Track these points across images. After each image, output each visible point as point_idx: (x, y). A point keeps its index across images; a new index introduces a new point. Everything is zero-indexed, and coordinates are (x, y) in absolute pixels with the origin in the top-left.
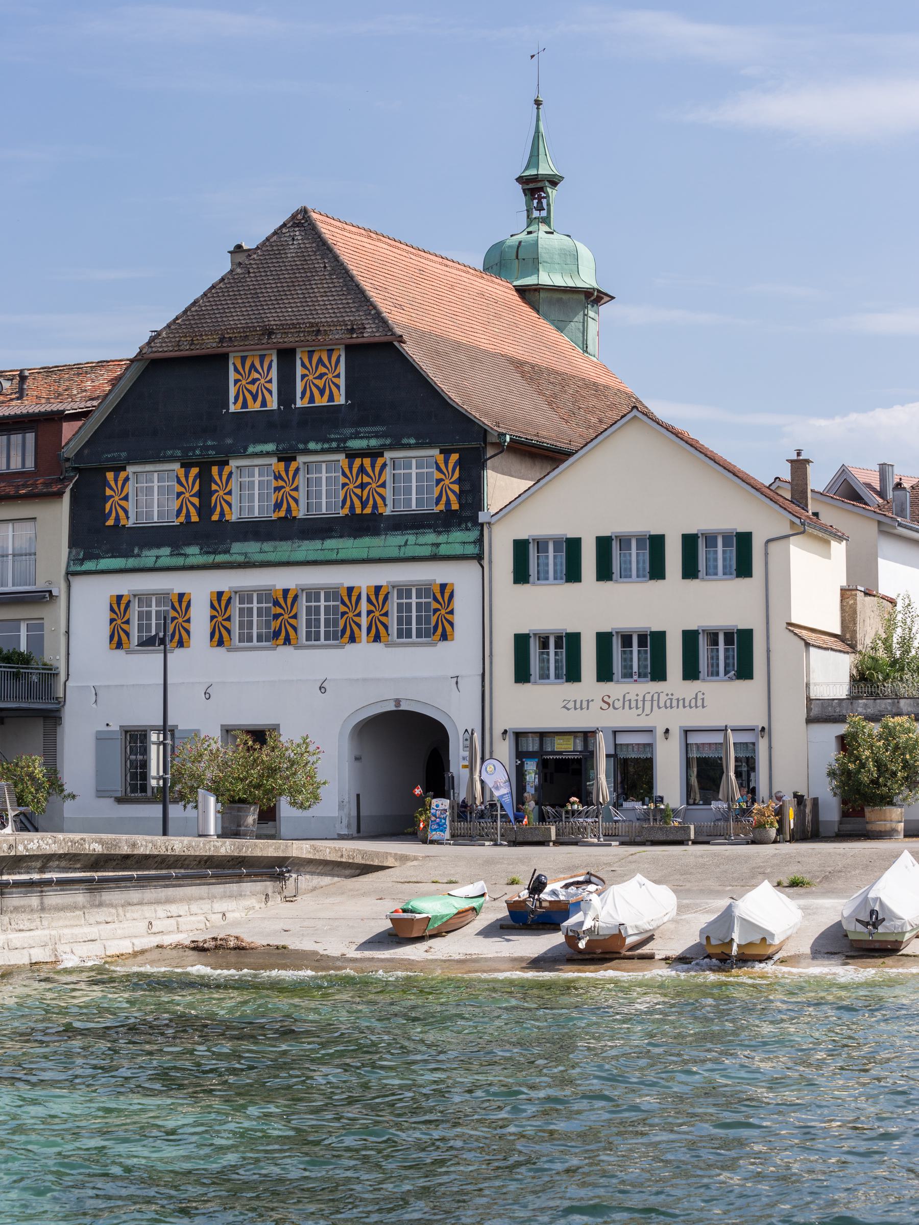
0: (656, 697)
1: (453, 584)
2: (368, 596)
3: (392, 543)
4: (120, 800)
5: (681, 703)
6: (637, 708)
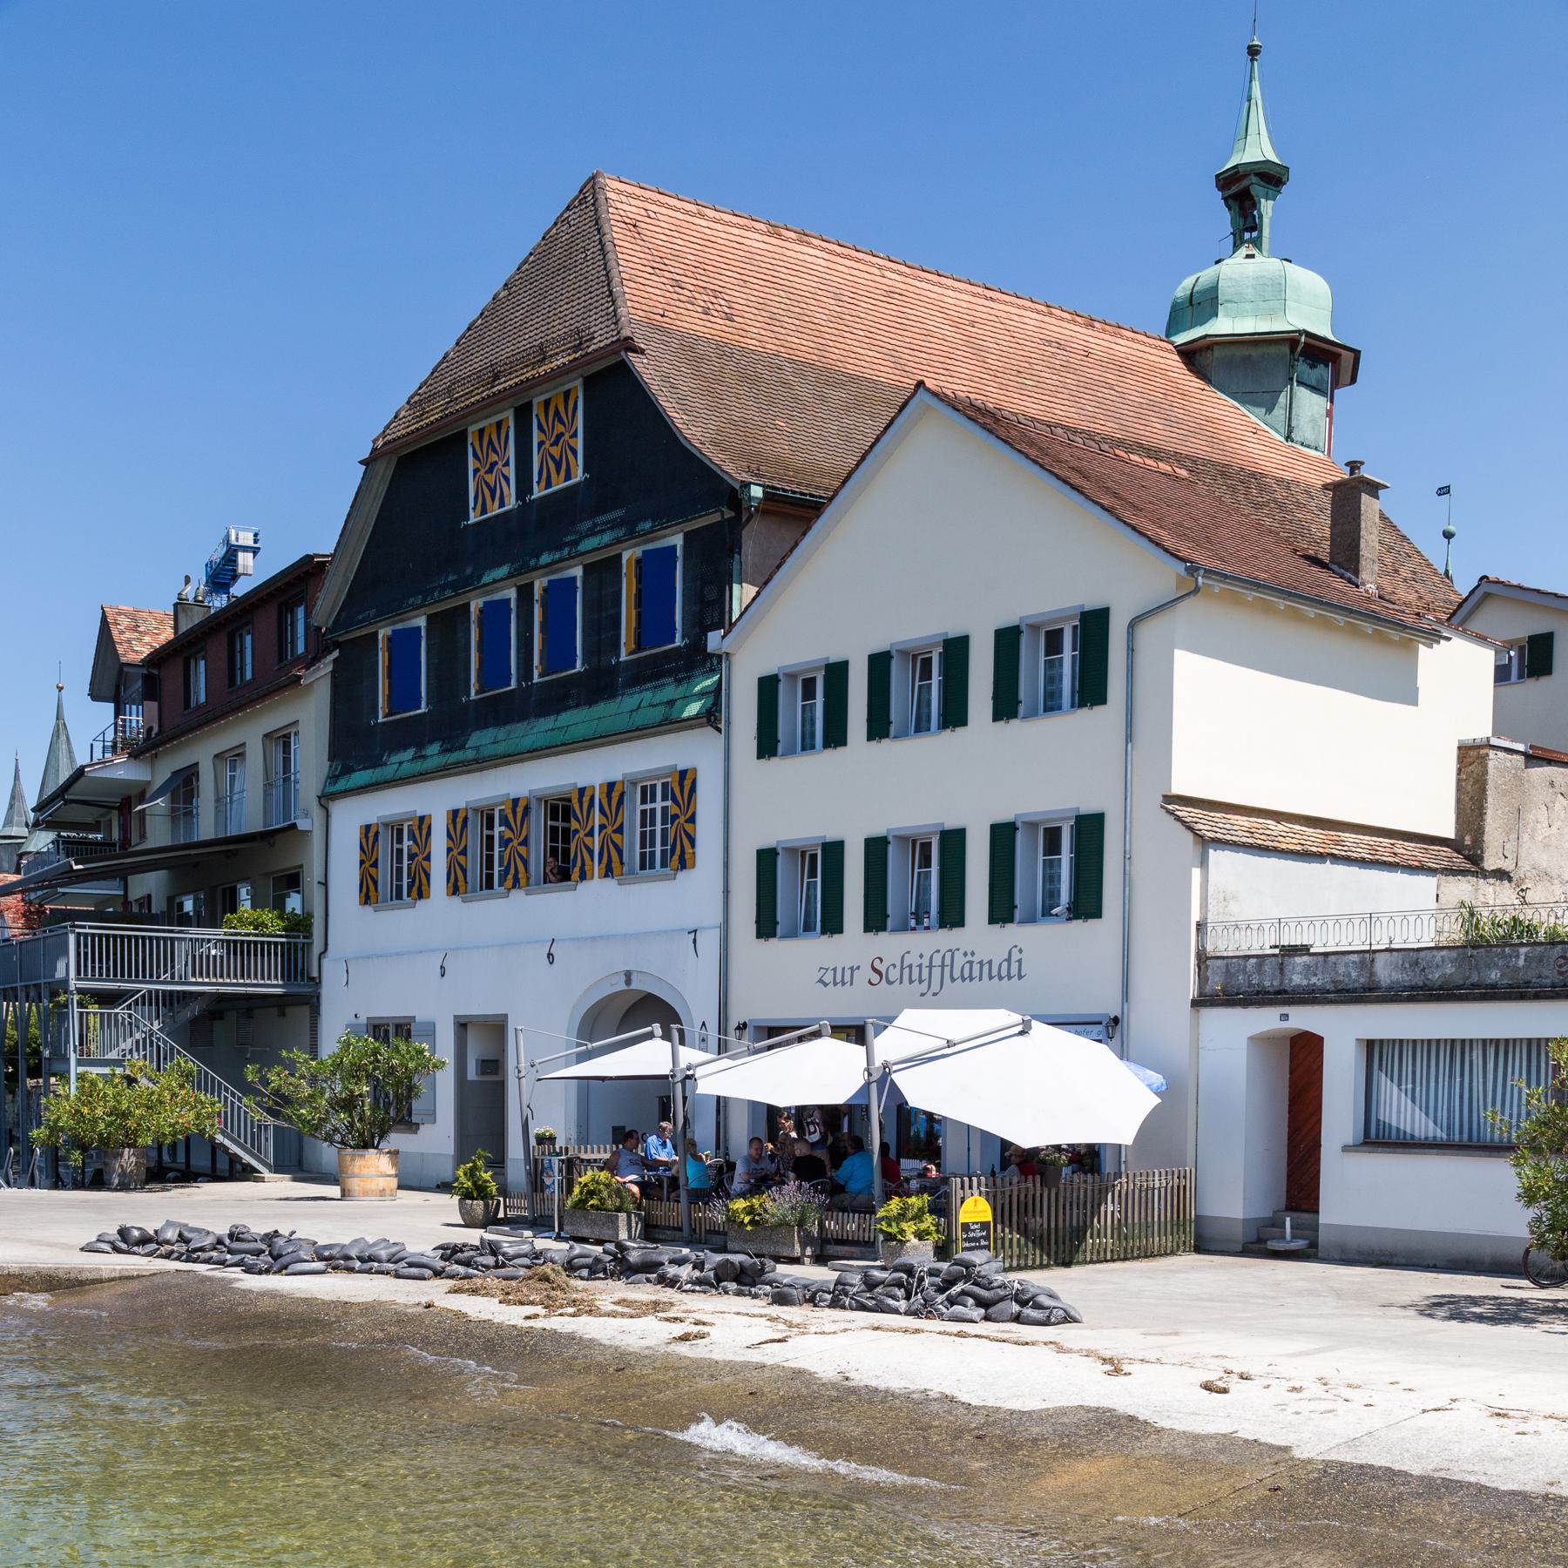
6: (921, 981)
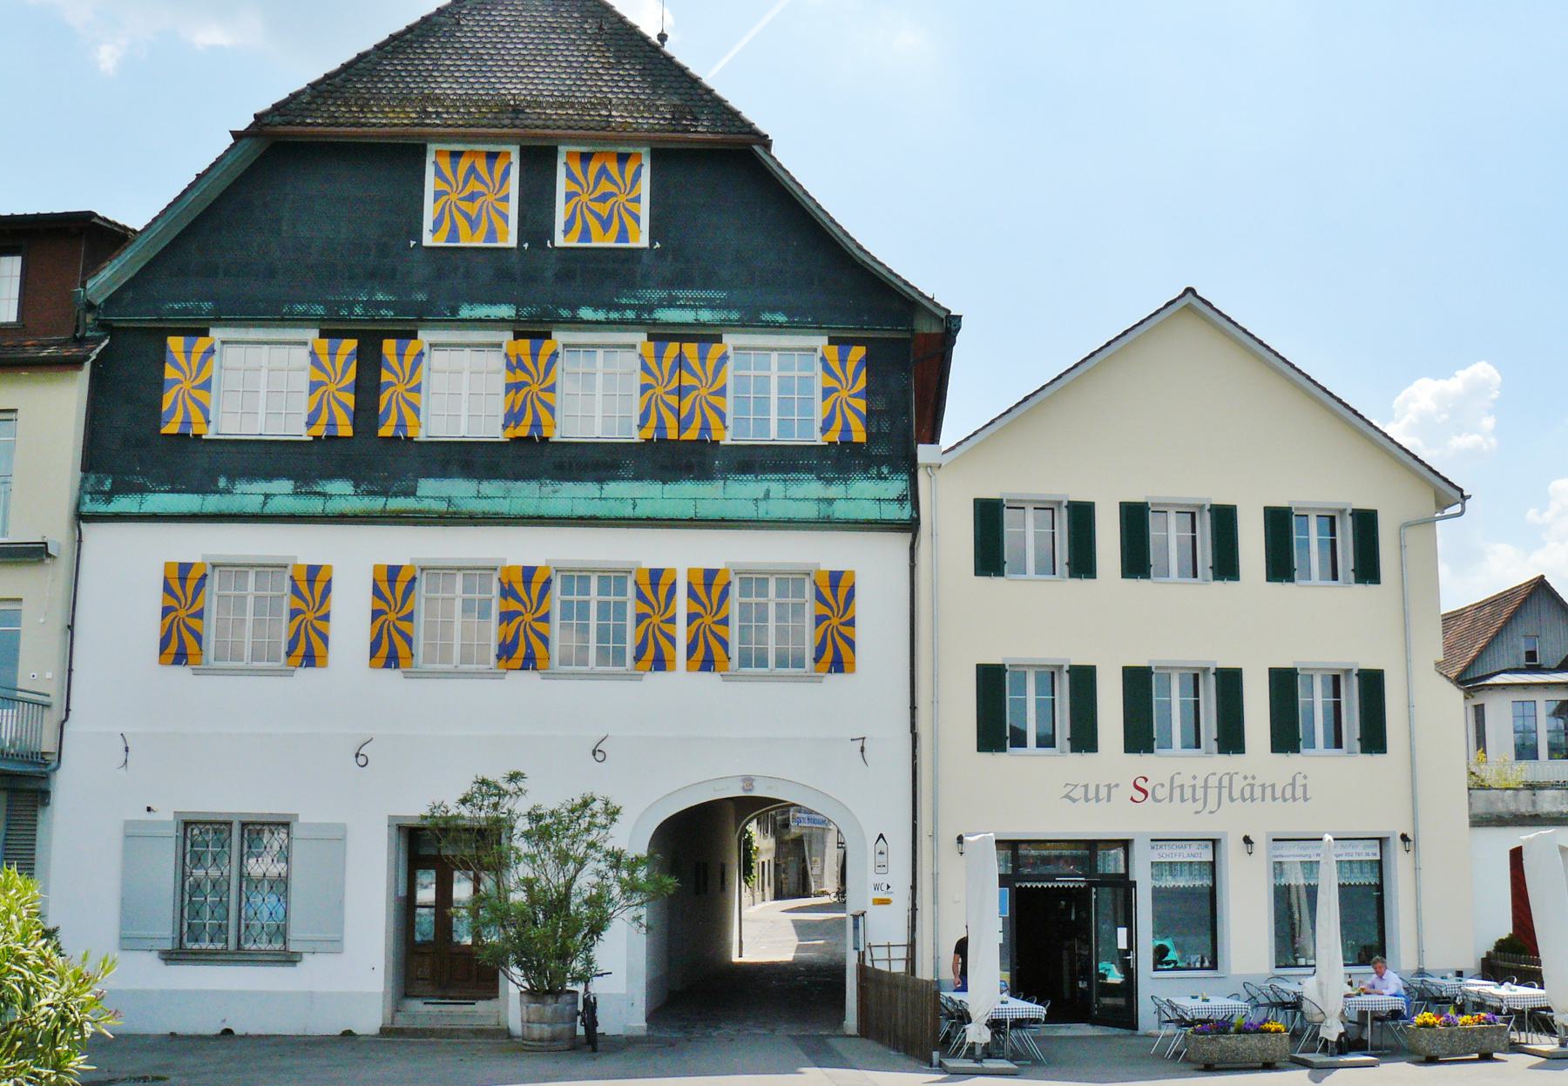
0: (1225, 782)
1: (852, 573)
2: (689, 584)
3: (740, 495)
4: (175, 956)
5: (1268, 791)
